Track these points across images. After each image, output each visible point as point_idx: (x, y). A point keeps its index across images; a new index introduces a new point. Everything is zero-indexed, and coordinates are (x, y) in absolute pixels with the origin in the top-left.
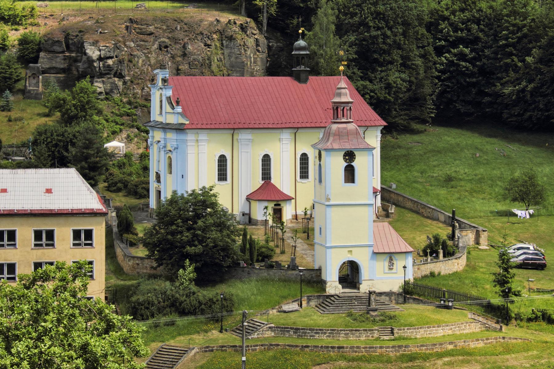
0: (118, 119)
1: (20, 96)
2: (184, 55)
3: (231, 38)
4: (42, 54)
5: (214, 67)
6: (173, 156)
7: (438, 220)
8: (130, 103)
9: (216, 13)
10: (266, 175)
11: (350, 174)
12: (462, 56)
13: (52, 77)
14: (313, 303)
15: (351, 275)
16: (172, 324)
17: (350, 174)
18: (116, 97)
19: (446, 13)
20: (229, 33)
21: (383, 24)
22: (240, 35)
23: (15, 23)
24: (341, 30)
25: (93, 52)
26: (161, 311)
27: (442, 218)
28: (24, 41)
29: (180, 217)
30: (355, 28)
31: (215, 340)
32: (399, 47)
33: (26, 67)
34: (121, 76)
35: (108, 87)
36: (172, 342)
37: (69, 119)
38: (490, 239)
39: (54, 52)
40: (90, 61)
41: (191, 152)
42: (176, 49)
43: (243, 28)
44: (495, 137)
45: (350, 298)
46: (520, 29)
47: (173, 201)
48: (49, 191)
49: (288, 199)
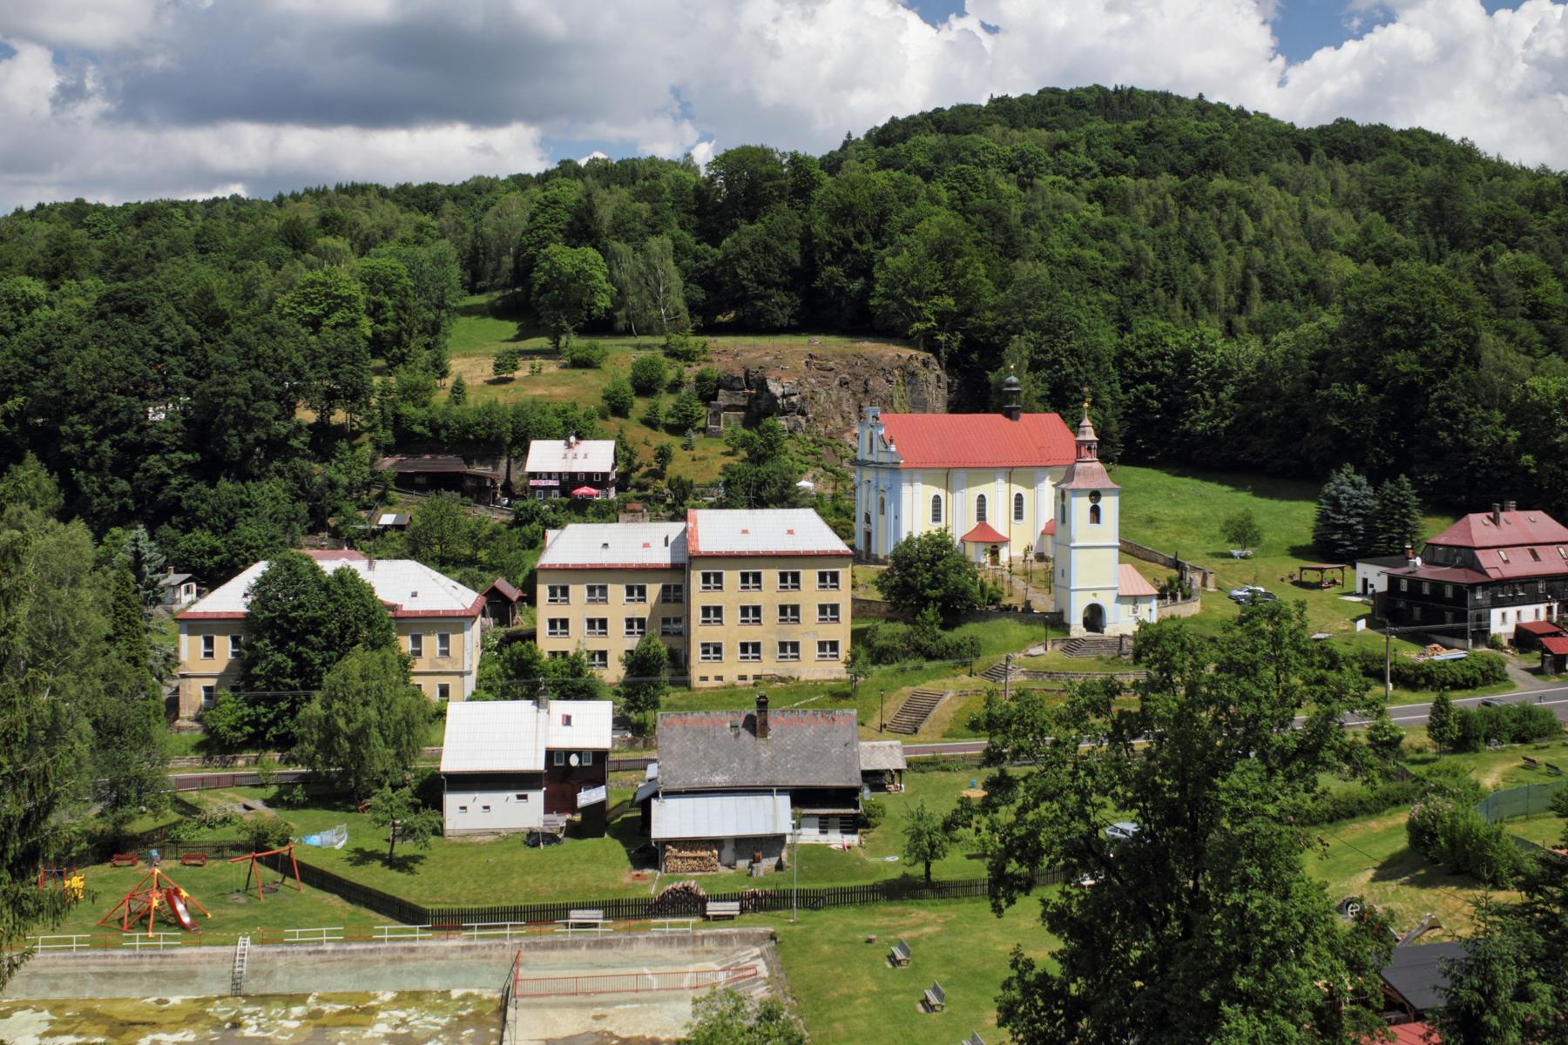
0: (804, 458)
1: (701, 435)
2: (866, 391)
3: (913, 374)
4: (721, 391)
5: (896, 405)
6: (886, 497)
7: (1155, 561)
8: (814, 441)
9: (895, 348)
10: (981, 515)
11: (1096, 513)
12: (1149, 393)
13: (731, 415)
14: (1058, 647)
15: (1094, 617)
16: (920, 668)
17: (1096, 513)
18: (800, 434)
19: (1132, 348)
20: (911, 368)
21: (1075, 360)
22: (922, 372)
23: (688, 359)
24: (1035, 366)
25: (775, 389)
26: (905, 654)
27: (1161, 560)
28: (701, 379)
29: (920, 560)
30: (1048, 365)
31: (967, 684)
32: (1090, 383)
33: (708, 405)
34: (804, 414)
35: (792, 425)
36: (923, 687)
37: (757, 459)
38: (1217, 582)
39: (733, 389)
40: (773, 398)
41: (906, 490)
42: (857, 386)
43: (925, 364)
44: (1211, 480)
45: (1096, 642)
46: (1209, 365)
47: (910, 541)
48: (790, 532)
49: (1005, 541)
